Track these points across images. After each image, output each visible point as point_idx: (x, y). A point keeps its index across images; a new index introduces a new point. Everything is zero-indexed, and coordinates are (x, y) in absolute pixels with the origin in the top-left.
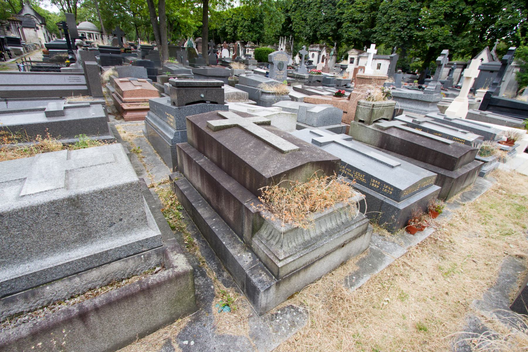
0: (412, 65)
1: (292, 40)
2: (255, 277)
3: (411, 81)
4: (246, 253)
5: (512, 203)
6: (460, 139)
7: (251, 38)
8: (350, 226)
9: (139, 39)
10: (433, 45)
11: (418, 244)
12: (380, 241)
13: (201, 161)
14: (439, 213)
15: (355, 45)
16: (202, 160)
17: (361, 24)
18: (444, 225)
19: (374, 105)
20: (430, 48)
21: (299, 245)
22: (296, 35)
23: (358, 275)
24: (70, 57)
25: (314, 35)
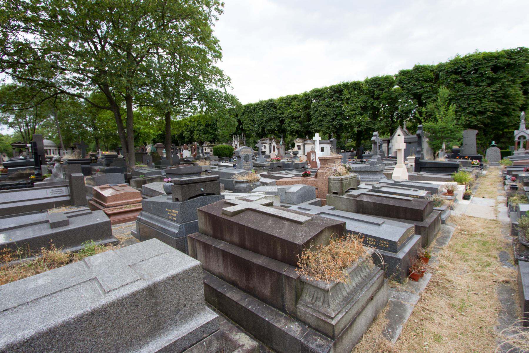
0: (347, 145)
1: (244, 137)
2: (312, 343)
3: (352, 157)
4: (293, 323)
5: (476, 240)
6: (415, 196)
7: (207, 139)
8: (372, 278)
9: (100, 150)
10: (359, 129)
11: (425, 289)
12: (394, 293)
13: (222, 245)
14: (429, 258)
15: (298, 135)
16: (222, 245)
17: (300, 119)
18: (437, 268)
19: (342, 179)
20: (358, 131)
21: (342, 302)
22: (247, 132)
23: (391, 327)
24: (36, 172)
25: (263, 131)
